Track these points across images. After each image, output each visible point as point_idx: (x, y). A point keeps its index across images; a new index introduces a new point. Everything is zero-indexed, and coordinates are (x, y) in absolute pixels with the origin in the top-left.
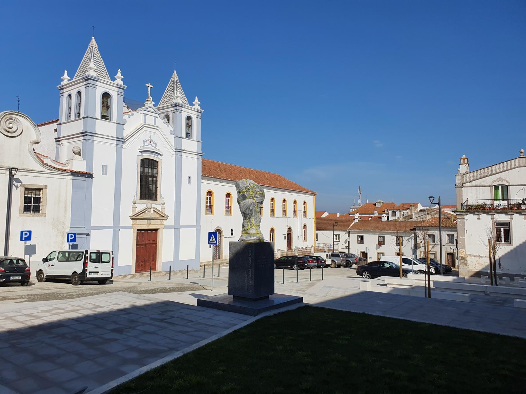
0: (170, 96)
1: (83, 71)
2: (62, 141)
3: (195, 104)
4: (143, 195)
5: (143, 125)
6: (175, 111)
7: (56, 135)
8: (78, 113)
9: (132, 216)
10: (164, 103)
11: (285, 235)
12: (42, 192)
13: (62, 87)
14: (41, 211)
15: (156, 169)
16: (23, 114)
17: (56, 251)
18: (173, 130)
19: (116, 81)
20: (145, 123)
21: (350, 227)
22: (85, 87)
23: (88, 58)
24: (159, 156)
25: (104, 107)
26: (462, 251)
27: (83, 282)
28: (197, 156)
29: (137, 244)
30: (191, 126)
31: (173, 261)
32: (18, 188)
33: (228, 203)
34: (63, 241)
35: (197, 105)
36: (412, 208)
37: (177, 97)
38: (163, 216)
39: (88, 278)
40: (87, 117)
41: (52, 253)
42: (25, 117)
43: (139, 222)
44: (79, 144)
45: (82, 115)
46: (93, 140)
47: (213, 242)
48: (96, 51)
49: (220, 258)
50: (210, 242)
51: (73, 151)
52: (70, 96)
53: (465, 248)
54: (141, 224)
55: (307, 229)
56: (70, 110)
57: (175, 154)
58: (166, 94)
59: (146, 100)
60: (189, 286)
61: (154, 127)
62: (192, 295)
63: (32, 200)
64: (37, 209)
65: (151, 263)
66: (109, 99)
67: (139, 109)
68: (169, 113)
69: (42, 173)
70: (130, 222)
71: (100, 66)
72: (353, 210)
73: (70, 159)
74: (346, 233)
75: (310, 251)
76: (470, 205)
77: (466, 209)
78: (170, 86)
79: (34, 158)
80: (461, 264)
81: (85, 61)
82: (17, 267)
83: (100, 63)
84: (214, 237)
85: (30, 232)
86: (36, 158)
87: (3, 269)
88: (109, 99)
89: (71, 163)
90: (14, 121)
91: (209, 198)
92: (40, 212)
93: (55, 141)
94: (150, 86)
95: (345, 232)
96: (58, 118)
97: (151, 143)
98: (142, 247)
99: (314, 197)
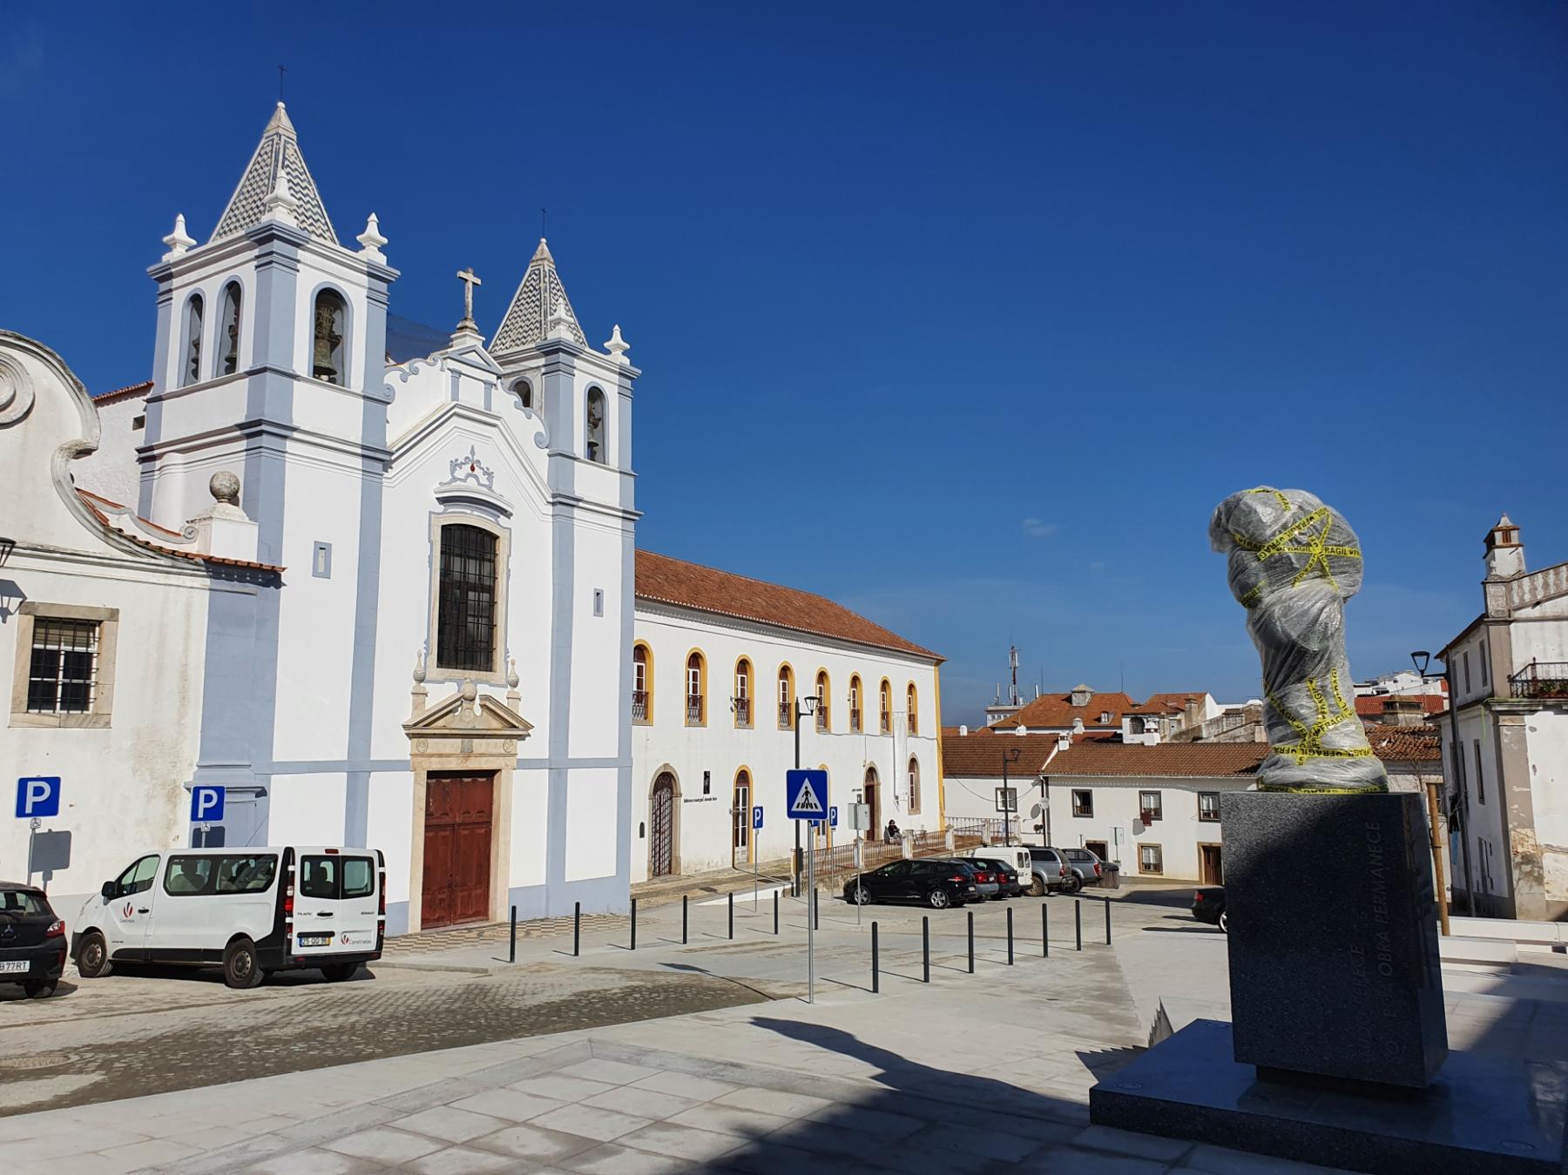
0: (528, 319)
2: (165, 457)
3: (610, 349)
4: (446, 652)
6: (551, 370)
7: (140, 438)
8: (227, 360)
10: (507, 345)
11: (859, 793)
12: (100, 633)
13: (170, 269)
14: (91, 706)
15: (490, 560)
16: (36, 342)
17: (157, 856)
18: (544, 433)
20: (456, 402)
21: (1046, 764)
22: (257, 267)
23: (264, 173)
24: (502, 516)
25: (323, 338)
26: (1522, 836)
27: (272, 973)
28: (620, 521)
29: (426, 826)
30: (599, 420)
31: (544, 883)
32: (9, 617)
33: (695, 687)
34: (172, 817)
35: (619, 352)
36: (1191, 707)
37: (558, 322)
38: (515, 727)
39: (297, 958)
40: (264, 370)
41: (141, 863)
43: (435, 745)
44: (231, 463)
45: (245, 363)
47: (809, 810)
48: (290, 151)
49: (670, 872)
50: (794, 809)
52: (196, 301)
53: (1533, 823)
54: (443, 752)
55: (918, 773)
56: (195, 350)
57: (551, 513)
58: (515, 315)
59: (458, 326)
60: (662, 980)
61: (486, 418)
62: (760, 1022)
63: (62, 663)
64: (77, 699)
65: (473, 894)
66: (337, 316)
67: (435, 355)
68: (528, 375)
69: (102, 562)
70: (404, 748)
71: (306, 199)
72: (993, 717)
73: (201, 517)
74: (1034, 785)
75: (944, 843)
76: (1544, 681)
77: (1526, 692)
78: (525, 289)
80: (1519, 879)
82: (15, 921)
83: (306, 192)
84: (810, 789)
85: (55, 783)
86: (80, 507)
88: (339, 311)
91: (694, 672)
92: (87, 709)
93: (136, 458)
94: (470, 277)
95: (1032, 781)
96: (150, 376)
97: (475, 472)
98: (444, 837)
99: (935, 671)
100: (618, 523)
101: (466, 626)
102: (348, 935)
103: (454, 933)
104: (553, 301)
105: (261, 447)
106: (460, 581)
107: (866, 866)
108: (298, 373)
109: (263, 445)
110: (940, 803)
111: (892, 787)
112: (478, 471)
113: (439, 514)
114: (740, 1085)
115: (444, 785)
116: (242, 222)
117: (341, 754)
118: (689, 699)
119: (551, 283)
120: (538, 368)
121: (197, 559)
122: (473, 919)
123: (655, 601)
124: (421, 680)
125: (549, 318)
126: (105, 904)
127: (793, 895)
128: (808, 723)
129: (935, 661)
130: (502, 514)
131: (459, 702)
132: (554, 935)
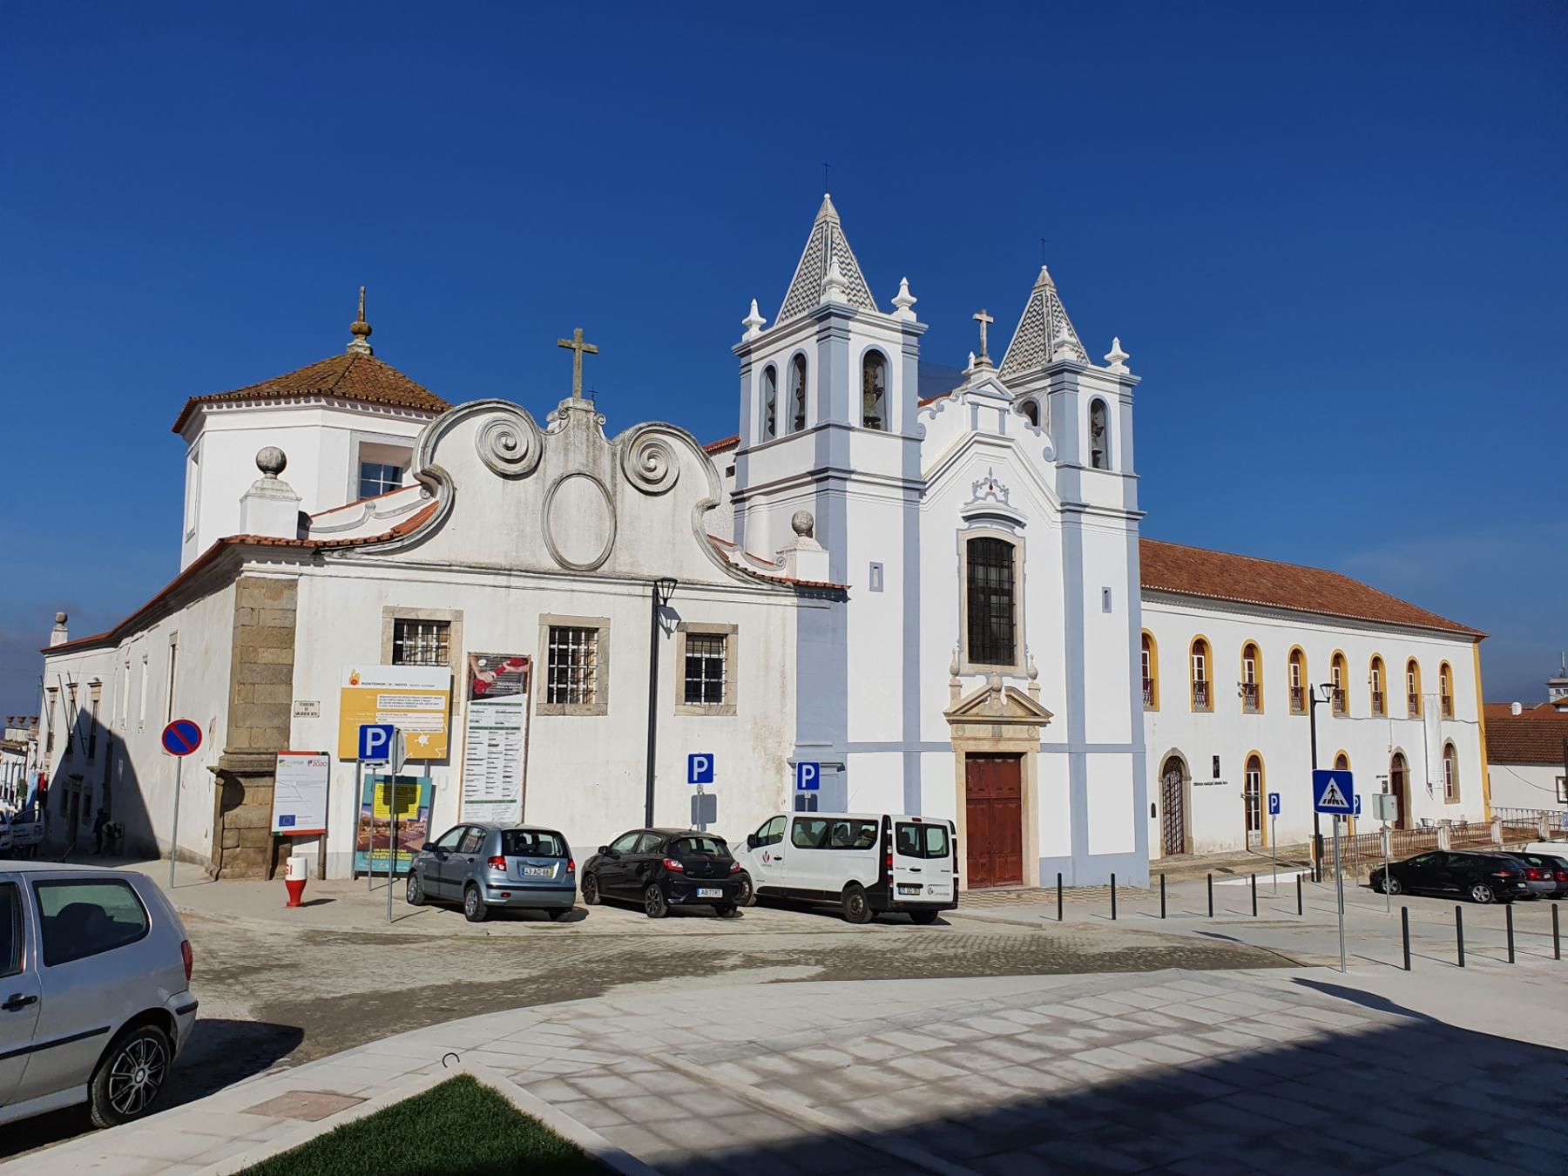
0: (1033, 343)
1: (804, 295)
2: (752, 499)
5: (972, 438)
6: (1057, 389)
7: (731, 484)
8: (770, 420)
9: (951, 711)
10: (1014, 368)
11: (1384, 779)
14: (723, 698)
16: (679, 428)
17: (785, 817)
19: (895, 313)
22: (818, 341)
24: (1017, 527)
30: (1102, 428)
32: (672, 634)
33: (1200, 672)
34: (780, 785)
35: (1119, 363)
37: (1061, 344)
38: (1037, 715)
39: (897, 903)
40: (828, 426)
41: (773, 821)
42: (683, 436)
43: (971, 730)
44: (805, 503)
45: (812, 421)
46: (846, 492)
47: (1335, 805)
49: (1182, 851)
50: (1321, 804)
51: (793, 525)
52: (771, 371)
54: (977, 736)
55: (1456, 759)
58: (1020, 340)
60: (1199, 944)
61: (1002, 441)
63: (704, 667)
64: (714, 694)
66: (879, 370)
67: (956, 391)
68: (1035, 395)
69: (726, 589)
70: (945, 732)
73: (788, 549)
75: (1489, 835)
78: (1029, 315)
79: (706, 550)
81: (808, 265)
83: (850, 267)
84: (1336, 788)
85: (710, 757)
87: (680, 866)
88: (880, 367)
89: (792, 559)
90: (660, 451)
91: (1198, 658)
94: (985, 318)
98: (982, 809)
100: (1123, 524)
101: (990, 626)
102: (933, 888)
103: (996, 894)
104: (1056, 323)
105: (828, 490)
106: (984, 588)
107: (1395, 855)
108: (853, 425)
109: (830, 488)
110: (1484, 792)
111: (1423, 773)
112: (995, 490)
113: (964, 530)
114: (1299, 1004)
115: (980, 764)
116: (802, 301)
117: (898, 737)
118: (1194, 685)
119: (1053, 306)
120: (1044, 388)
121: (788, 583)
122: (1010, 882)
123: (1156, 590)
124: (956, 674)
125: (1053, 342)
126: (749, 851)
127: (1313, 881)
128: (1324, 711)
129: (1474, 638)
130: (1017, 525)
131: (988, 694)
132: (1084, 901)
